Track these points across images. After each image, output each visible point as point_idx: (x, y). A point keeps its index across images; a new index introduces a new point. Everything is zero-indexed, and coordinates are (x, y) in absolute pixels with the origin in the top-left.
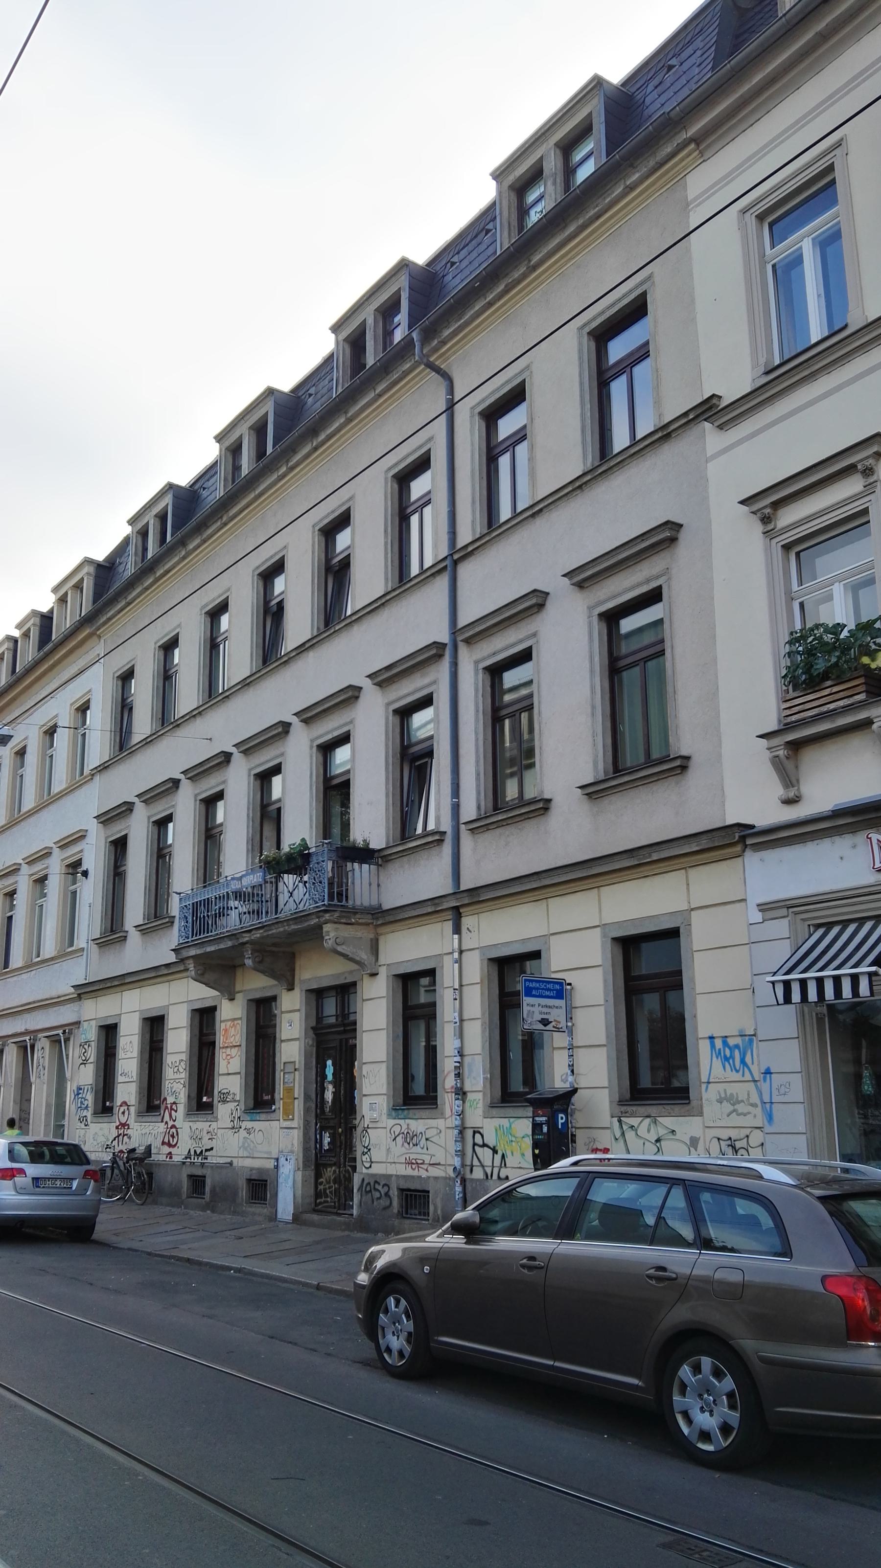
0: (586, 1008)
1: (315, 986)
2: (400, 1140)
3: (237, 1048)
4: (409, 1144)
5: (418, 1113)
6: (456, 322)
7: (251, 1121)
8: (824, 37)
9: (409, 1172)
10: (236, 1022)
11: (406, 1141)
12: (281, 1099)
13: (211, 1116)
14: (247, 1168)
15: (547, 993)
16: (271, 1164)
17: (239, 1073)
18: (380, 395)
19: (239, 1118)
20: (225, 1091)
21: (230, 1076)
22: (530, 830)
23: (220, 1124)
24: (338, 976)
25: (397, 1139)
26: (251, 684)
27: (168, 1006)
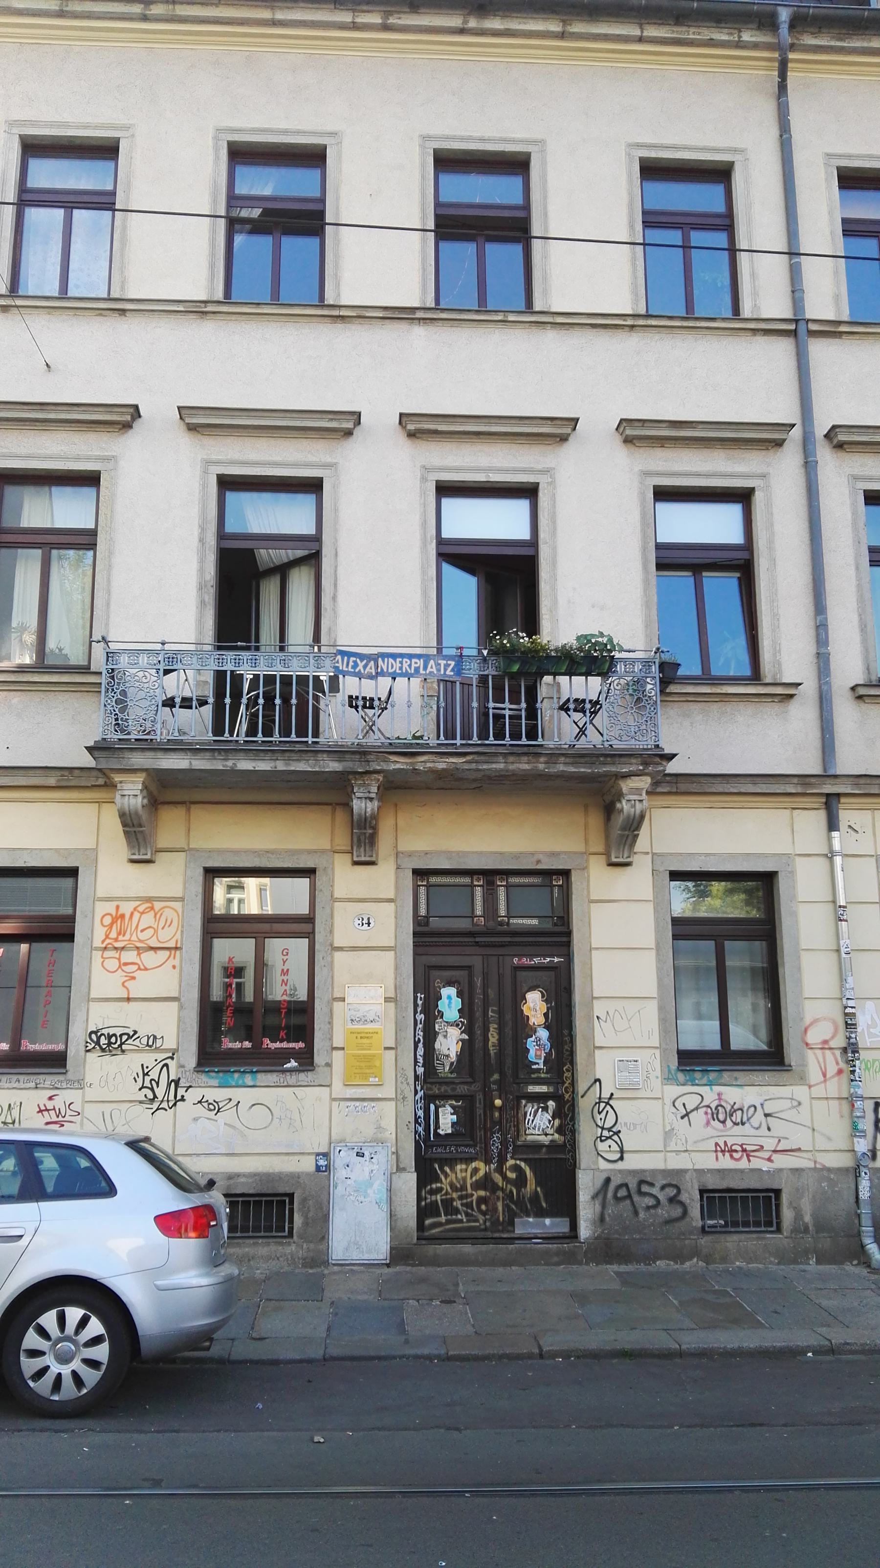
0: (870, 952)
2: (699, 1117)
4: (724, 1122)
5: (742, 1077)
6: (832, 38)
9: (726, 1162)
10: (158, 905)
13: (61, 1078)
19: (177, 1082)
23: (90, 1094)
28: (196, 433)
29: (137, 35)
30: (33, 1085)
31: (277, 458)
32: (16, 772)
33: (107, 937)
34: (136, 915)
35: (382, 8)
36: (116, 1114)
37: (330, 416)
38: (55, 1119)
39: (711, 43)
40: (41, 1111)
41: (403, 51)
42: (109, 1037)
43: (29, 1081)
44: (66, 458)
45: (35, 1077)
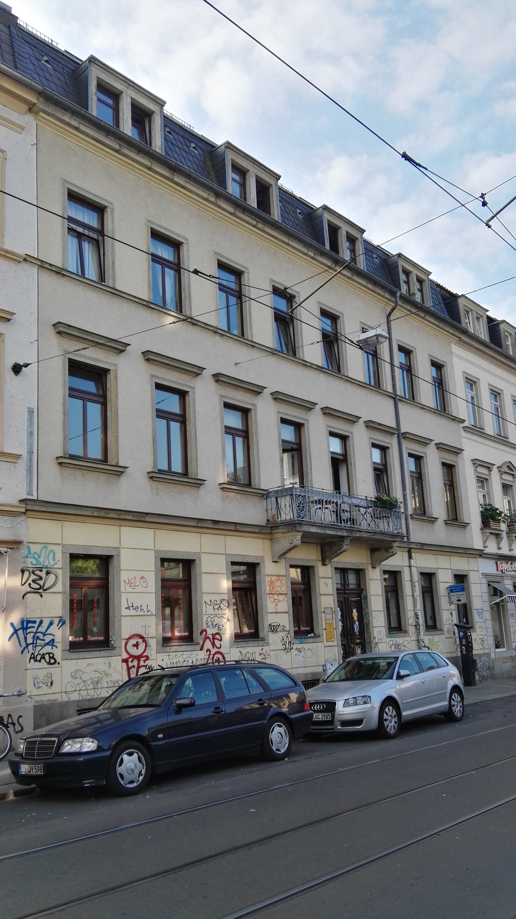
1: (341, 566)
3: (283, 596)
7: (300, 643)
8: (494, 358)
10: (281, 578)
11: (396, 648)
12: (324, 629)
14: (303, 674)
15: (459, 590)
16: (321, 669)
17: (287, 612)
18: (365, 287)
19: (290, 642)
20: (275, 624)
21: (278, 614)
22: (427, 526)
23: (272, 647)
24: (355, 564)
25: (392, 647)
26: (275, 355)
27: (155, 551)
28: (59, 335)
29: (249, 230)
30: (257, 645)
31: (294, 414)
32: (175, 518)
33: (270, 590)
34: (276, 582)
35: (315, 252)
36: (278, 654)
37: (311, 404)
38: (264, 657)
39: (379, 294)
40: (260, 655)
41: (312, 267)
42: (274, 626)
43: (256, 644)
44: (243, 402)
45: (257, 642)
